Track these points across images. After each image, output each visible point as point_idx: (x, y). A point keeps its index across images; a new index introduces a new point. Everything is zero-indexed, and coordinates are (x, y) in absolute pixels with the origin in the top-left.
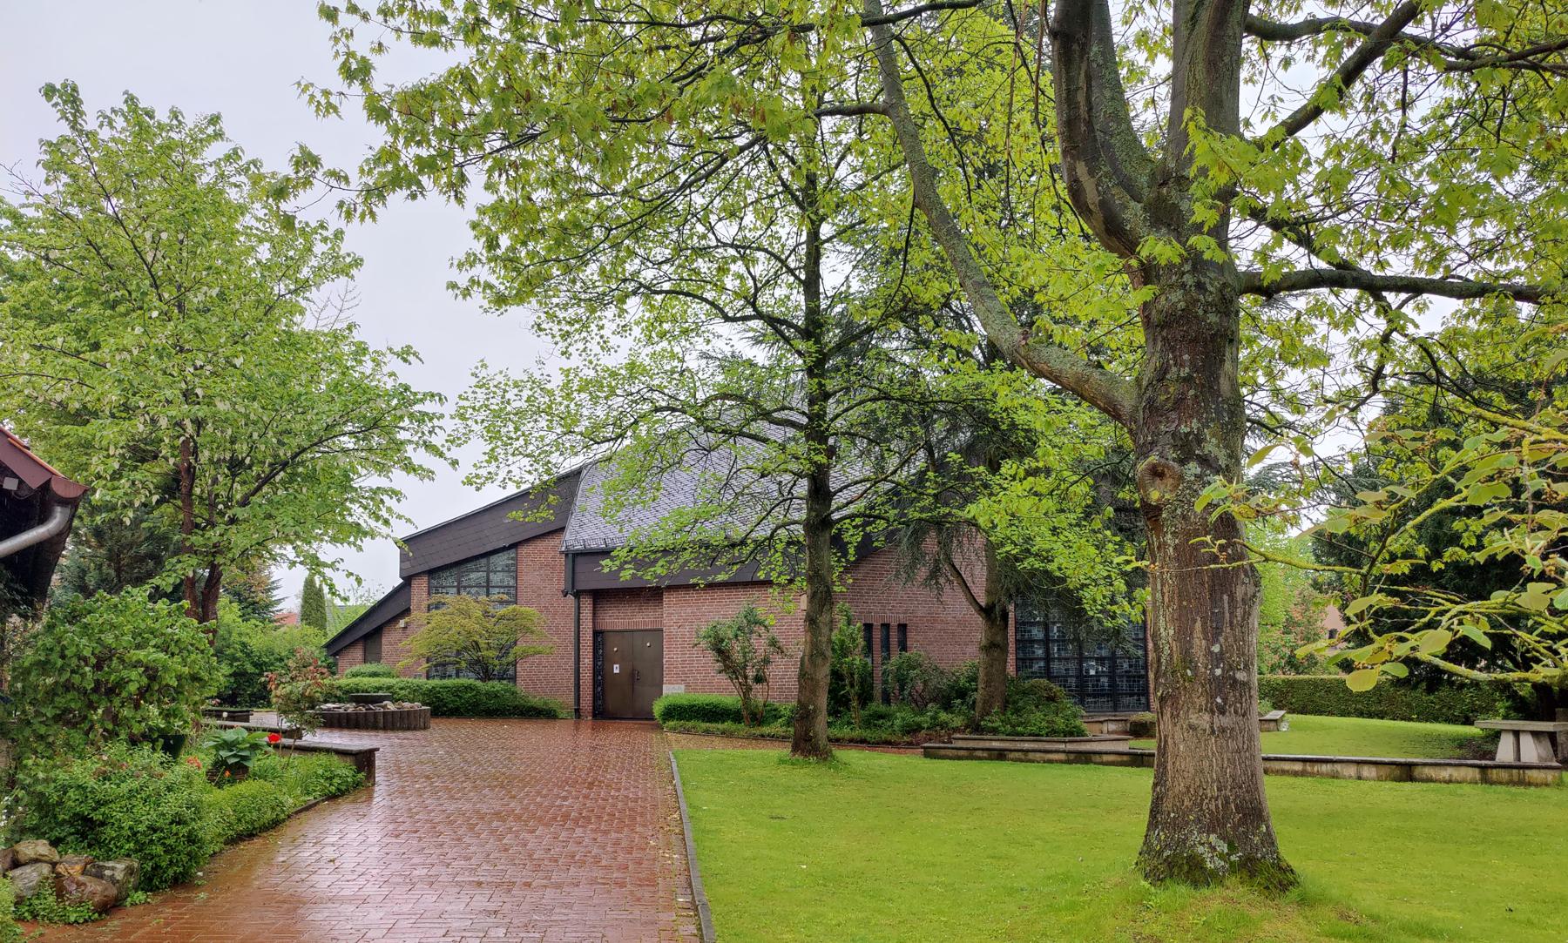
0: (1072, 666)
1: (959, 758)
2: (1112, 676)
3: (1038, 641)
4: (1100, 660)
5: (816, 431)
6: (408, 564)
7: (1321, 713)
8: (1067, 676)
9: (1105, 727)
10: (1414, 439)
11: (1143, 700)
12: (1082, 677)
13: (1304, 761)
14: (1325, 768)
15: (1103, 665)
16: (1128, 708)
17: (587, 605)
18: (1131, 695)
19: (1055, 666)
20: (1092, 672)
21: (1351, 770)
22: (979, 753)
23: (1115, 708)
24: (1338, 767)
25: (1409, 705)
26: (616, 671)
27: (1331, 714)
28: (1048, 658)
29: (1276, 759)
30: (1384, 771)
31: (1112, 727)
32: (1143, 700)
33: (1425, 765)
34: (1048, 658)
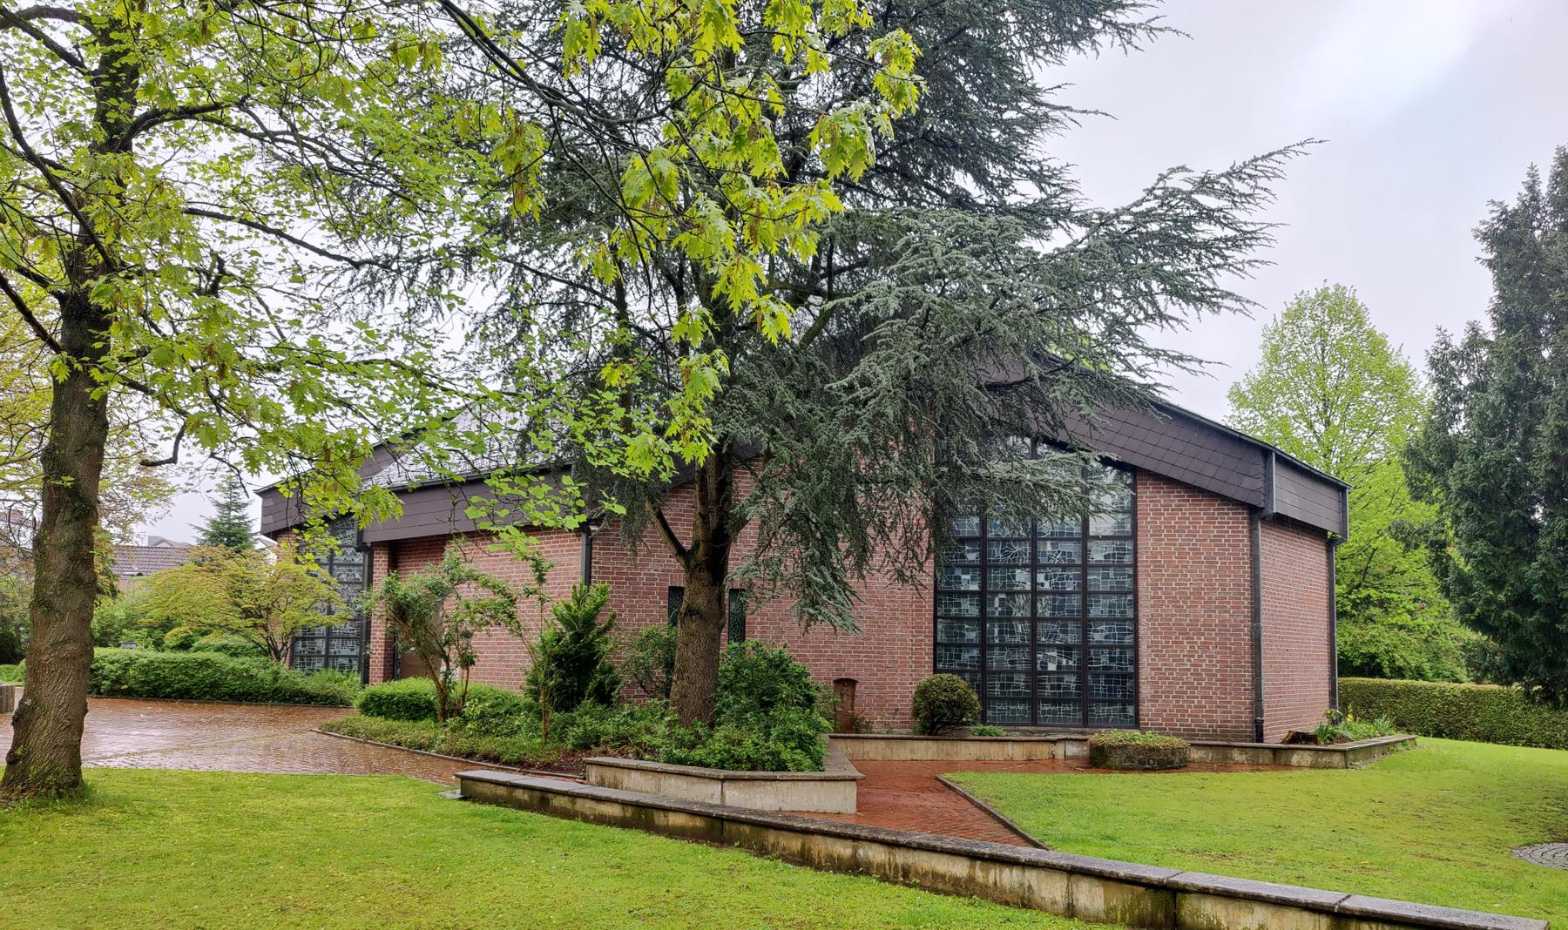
0: (1021, 657)
2: (1082, 671)
3: (970, 620)
4: (1066, 649)
6: (270, 519)
7: (1454, 735)
8: (1013, 671)
9: (1059, 750)
10: (126, 53)
11: (1131, 710)
12: (1035, 675)
14: (1009, 878)
15: (1068, 656)
16: (1106, 723)
17: (381, 561)
18: (1112, 703)
20: (1052, 667)
21: (1052, 889)
22: (519, 794)
23: (1086, 722)
24: (1031, 877)
25: (329, 660)
27: (1530, 743)
28: (984, 645)
29: (921, 848)
30: (1121, 898)
31: (1072, 749)
32: (1131, 710)
33: (1204, 892)
34: (984, 645)
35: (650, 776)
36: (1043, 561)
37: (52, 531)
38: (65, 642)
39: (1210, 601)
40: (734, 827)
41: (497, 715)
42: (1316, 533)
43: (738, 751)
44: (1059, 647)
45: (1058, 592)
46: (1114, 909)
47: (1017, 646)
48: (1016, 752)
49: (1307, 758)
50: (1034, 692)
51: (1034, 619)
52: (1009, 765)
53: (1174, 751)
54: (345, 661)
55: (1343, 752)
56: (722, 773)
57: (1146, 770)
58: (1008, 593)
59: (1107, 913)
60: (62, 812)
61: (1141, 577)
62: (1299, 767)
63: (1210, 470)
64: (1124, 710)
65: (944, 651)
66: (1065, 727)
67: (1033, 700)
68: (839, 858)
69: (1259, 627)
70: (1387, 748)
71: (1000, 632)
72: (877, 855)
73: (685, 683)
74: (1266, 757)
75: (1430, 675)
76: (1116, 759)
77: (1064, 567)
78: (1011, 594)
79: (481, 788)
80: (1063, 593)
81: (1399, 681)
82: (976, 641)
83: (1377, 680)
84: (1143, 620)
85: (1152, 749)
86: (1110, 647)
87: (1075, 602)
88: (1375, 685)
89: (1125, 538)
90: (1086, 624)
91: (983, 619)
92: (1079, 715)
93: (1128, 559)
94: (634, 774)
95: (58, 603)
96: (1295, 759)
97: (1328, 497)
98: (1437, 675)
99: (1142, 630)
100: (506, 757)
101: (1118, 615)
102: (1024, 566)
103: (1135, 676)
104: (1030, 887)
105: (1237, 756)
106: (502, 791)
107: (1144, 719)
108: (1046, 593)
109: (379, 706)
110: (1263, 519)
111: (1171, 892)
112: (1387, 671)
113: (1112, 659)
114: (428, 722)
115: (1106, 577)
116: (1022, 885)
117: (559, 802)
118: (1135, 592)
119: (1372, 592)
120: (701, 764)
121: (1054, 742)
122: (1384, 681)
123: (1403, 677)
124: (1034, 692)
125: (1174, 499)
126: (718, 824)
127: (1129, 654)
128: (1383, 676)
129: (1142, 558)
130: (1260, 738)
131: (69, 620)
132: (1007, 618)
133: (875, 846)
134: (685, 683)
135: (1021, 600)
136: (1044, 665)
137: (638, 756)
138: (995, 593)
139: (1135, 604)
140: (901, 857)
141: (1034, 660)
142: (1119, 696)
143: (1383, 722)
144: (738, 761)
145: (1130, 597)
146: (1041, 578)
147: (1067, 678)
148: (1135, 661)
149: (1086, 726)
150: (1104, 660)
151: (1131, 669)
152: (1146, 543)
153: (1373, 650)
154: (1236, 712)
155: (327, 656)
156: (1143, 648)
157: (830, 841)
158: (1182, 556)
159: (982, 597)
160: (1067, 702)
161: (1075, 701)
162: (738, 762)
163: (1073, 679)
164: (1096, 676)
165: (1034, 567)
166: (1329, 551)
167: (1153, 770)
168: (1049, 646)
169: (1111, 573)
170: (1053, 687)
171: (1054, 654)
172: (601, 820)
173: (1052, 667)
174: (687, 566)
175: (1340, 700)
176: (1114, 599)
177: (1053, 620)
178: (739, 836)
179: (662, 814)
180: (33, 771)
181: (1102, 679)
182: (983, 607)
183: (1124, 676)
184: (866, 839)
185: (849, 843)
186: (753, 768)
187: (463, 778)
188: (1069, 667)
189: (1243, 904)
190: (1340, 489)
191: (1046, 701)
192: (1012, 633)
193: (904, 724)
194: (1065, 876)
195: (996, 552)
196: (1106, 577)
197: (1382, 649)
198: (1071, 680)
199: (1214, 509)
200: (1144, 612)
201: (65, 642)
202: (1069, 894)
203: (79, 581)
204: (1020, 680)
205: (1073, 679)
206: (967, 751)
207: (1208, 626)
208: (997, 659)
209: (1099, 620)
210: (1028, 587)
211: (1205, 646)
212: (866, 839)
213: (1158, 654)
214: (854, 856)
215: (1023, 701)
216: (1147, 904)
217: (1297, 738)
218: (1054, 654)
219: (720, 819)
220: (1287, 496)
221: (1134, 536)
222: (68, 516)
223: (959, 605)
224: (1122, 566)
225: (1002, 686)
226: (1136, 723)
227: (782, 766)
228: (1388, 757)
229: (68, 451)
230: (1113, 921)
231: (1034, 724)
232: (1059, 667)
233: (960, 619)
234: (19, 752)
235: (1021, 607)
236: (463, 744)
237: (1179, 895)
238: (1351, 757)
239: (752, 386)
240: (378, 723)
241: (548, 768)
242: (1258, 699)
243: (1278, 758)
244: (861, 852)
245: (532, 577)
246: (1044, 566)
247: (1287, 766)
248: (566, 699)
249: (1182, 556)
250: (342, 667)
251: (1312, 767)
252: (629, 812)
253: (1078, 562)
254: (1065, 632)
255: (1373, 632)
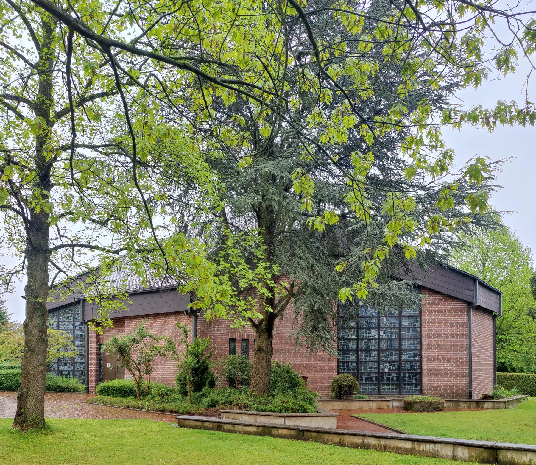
0: (374, 366)
1: (196, 427)
2: (399, 372)
4: (392, 363)
5: (41, 108)
9: (390, 404)
11: (419, 387)
12: (380, 373)
13: (414, 440)
14: (429, 447)
15: (393, 366)
16: (409, 393)
18: (411, 384)
19: (363, 366)
21: (448, 451)
22: (207, 424)
23: (400, 392)
24: (438, 447)
26: (108, 366)
30: (475, 453)
31: (396, 404)
32: (419, 387)
33: (509, 449)
34: (358, 361)
35: (251, 417)
36: (383, 326)
37: (32, 320)
38: (39, 365)
39: (451, 342)
40: (309, 434)
41: (165, 395)
42: (488, 312)
43: (286, 406)
44: (389, 362)
45: (389, 339)
46: (472, 457)
47: (372, 361)
48: (374, 405)
49: (490, 405)
50: (379, 381)
51: (379, 350)
52: (371, 410)
53: (439, 404)
54: (67, 373)
55: (505, 402)
56: (285, 415)
57: (429, 411)
58: (368, 340)
59: (469, 458)
60: (45, 434)
61: (423, 332)
62: (487, 409)
63: (452, 287)
64: (416, 387)
65: (342, 365)
66: (392, 394)
67: (379, 384)
68: (356, 443)
69: (471, 352)
70: (518, 400)
71: (365, 356)
72: (373, 441)
73: (258, 379)
74: (474, 405)
75: (526, 371)
76: (416, 407)
77: (392, 328)
78: (370, 340)
79: (188, 422)
80: (391, 339)
81: (514, 373)
82: (355, 360)
83: (505, 373)
84: (424, 350)
85: (431, 403)
86: (410, 361)
87: (396, 342)
88: (505, 375)
89: (415, 316)
90: (400, 352)
91: (357, 351)
92: (398, 390)
93: (417, 325)
94: (244, 416)
95: (36, 349)
96: (486, 405)
97: (494, 296)
98: (529, 371)
99: (424, 354)
100: (181, 411)
101: (413, 348)
102: (375, 328)
103: (421, 373)
104: (438, 450)
105: (462, 405)
106: (199, 423)
107: (424, 391)
108: (384, 339)
109: (108, 391)
110: (473, 308)
111: (495, 449)
112: (509, 369)
113: (411, 366)
114: (131, 398)
115: (409, 332)
116: (434, 450)
117: (226, 427)
118: (421, 338)
119: (503, 336)
120: (271, 411)
121: (388, 401)
122: (508, 373)
123: (515, 372)
124: (379, 381)
125: (437, 299)
126: (302, 432)
127: (418, 364)
128: (507, 371)
129: (424, 324)
130: (471, 397)
131: (40, 357)
132: (368, 350)
133: (371, 438)
134: (258, 379)
135: (373, 342)
136: (383, 369)
137: (240, 409)
138: (363, 340)
139: (421, 343)
140: (383, 442)
141: (379, 366)
142: (414, 382)
143: (515, 390)
144: (288, 410)
145: (418, 340)
146: (382, 333)
147: (392, 374)
148: (421, 367)
149: (400, 394)
150: (408, 367)
151: (419, 370)
152: (425, 318)
153: (503, 361)
154: (462, 388)
155: (58, 371)
156: (424, 361)
157: (352, 437)
158: (440, 323)
159: (358, 341)
160: (393, 384)
161: (396, 384)
162: (287, 410)
163: (395, 375)
164: (405, 373)
165: (379, 328)
166: (494, 320)
167: (432, 411)
168: (385, 361)
169: (411, 330)
170: (387, 378)
171: (387, 365)
172: (248, 433)
173: (386, 370)
174: (258, 331)
175: (497, 381)
176: (412, 341)
177: (387, 350)
178: (311, 437)
179: (275, 430)
180: (29, 418)
181: (407, 375)
182: (358, 345)
183: (416, 373)
184: (369, 436)
185: (360, 437)
186: (294, 412)
187: (179, 419)
188: (393, 370)
189: (523, 452)
190: (499, 294)
191: (384, 384)
192: (370, 356)
193: (326, 395)
194: (452, 446)
195: (363, 322)
196: (409, 332)
197: (507, 360)
198: (394, 375)
199: (453, 303)
200: (424, 347)
201: (39, 365)
202: (454, 452)
203: (43, 340)
204: (374, 376)
205: (395, 375)
206: (354, 405)
207: (450, 352)
208: (364, 367)
209: (406, 350)
210: (376, 337)
211: (449, 360)
212: (369, 436)
213: (430, 364)
214: (363, 442)
215: (374, 384)
216: (485, 454)
217: (486, 397)
218: (387, 365)
219: (303, 431)
220: (483, 299)
221: (420, 315)
222: (39, 314)
223: (347, 345)
224: (415, 328)
225: (366, 378)
226: (421, 393)
227: (306, 411)
228: (519, 404)
229: (37, 287)
230: (472, 461)
231: (379, 394)
232: (389, 370)
233: (349, 351)
234: (23, 410)
235: (374, 346)
236: (160, 406)
237: (498, 451)
238: (507, 404)
239: (301, 258)
240: (105, 398)
241: (206, 415)
242: (470, 382)
243: (479, 405)
244: (366, 441)
245: (183, 336)
246: (383, 328)
247: (483, 408)
248: (198, 387)
249: (440, 323)
250: (66, 376)
251: (493, 408)
252: (260, 430)
253: (397, 326)
254: (392, 355)
255: (504, 353)
